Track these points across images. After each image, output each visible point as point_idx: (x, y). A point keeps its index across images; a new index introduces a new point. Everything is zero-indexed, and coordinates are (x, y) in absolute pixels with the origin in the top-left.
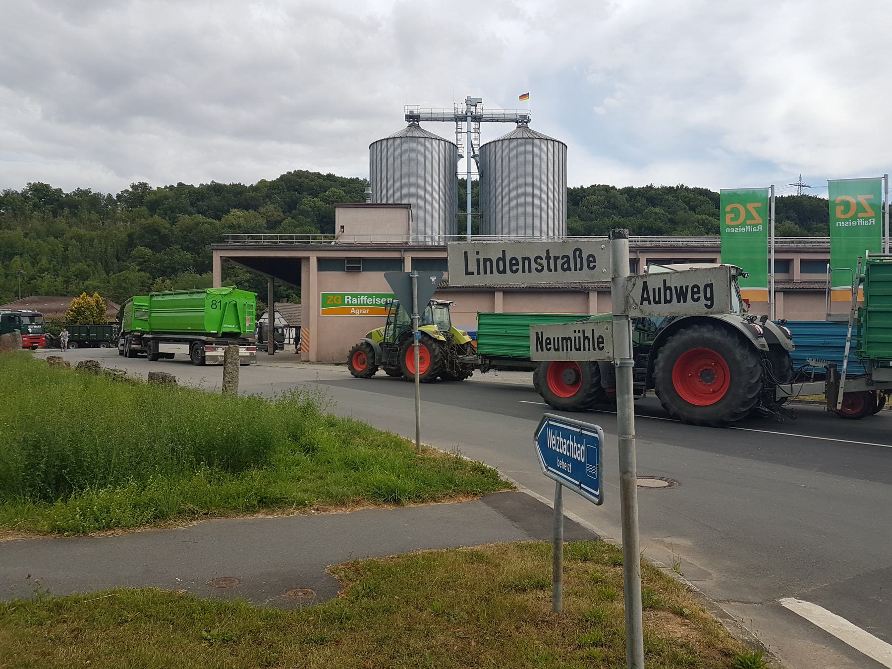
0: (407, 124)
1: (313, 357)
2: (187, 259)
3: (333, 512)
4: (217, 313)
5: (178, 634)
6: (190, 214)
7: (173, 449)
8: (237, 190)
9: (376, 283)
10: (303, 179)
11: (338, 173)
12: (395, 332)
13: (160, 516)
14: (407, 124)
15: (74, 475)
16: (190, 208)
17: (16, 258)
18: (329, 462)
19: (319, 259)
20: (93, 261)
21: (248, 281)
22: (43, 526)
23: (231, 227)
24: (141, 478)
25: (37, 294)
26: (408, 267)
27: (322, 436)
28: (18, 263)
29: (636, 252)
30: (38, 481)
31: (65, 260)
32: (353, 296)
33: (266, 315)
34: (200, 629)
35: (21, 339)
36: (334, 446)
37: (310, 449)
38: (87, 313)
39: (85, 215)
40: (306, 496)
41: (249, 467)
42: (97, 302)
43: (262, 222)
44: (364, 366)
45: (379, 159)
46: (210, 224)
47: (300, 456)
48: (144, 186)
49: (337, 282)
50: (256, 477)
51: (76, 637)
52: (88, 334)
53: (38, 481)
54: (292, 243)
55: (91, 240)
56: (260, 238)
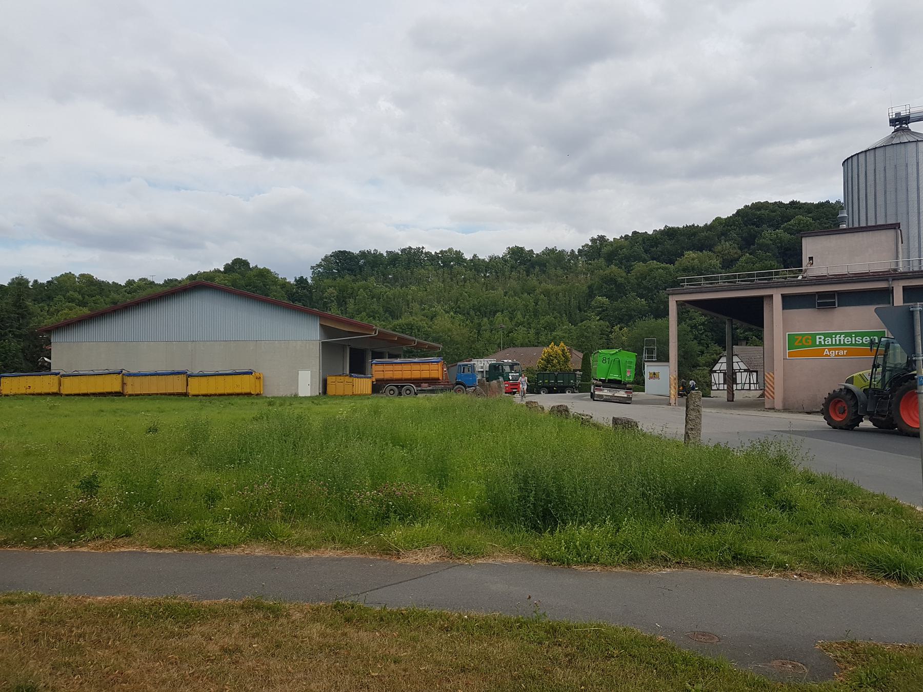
0: (893, 129)
1: (778, 404)
2: (642, 305)
3: (820, 580)
4: (606, 366)
5: (661, 681)
6: (645, 261)
7: (643, 494)
8: (691, 232)
9: (862, 320)
10: (763, 211)
11: (803, 199)
12: (883, 376)
13: (634, 560)
14: (893, 129)
15: (557, 510)
16: (644, 256)
17: (498, 314)
18: (811, 524)
19: (783, 296)
20: (559, 313)
21: (703, 324)
22: (535, 553)
23: (686, 270)
24: (617, 521)
25: (515, 346)
26: (898, 299)
27: (800, 493)
28: (500, 319)
29: (887, 280)
30: (529, 512)
31: (536, 314)
32: (826, 335)
33: (723, 360)
34: (684, 680)
35: (504, 385)
36: (815, 506)
37: (787, 506)
38: (555, 361)
39: (552, 271)
40: (786, 558)
41: (721, 520)
42: (563, 350)
43: (716, 262)
44: (844, 416)
45: (855, 176)
46: (663, 268)
47: (775, 512)
48: (602, 238)
49: (806, 321)
50: (729, 531)
51: (570, 661)
52: (556, 381)
53: (529, 512)
54: (786, 278)
55: (557, 294)
56: (716, 279)
